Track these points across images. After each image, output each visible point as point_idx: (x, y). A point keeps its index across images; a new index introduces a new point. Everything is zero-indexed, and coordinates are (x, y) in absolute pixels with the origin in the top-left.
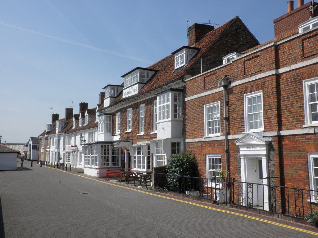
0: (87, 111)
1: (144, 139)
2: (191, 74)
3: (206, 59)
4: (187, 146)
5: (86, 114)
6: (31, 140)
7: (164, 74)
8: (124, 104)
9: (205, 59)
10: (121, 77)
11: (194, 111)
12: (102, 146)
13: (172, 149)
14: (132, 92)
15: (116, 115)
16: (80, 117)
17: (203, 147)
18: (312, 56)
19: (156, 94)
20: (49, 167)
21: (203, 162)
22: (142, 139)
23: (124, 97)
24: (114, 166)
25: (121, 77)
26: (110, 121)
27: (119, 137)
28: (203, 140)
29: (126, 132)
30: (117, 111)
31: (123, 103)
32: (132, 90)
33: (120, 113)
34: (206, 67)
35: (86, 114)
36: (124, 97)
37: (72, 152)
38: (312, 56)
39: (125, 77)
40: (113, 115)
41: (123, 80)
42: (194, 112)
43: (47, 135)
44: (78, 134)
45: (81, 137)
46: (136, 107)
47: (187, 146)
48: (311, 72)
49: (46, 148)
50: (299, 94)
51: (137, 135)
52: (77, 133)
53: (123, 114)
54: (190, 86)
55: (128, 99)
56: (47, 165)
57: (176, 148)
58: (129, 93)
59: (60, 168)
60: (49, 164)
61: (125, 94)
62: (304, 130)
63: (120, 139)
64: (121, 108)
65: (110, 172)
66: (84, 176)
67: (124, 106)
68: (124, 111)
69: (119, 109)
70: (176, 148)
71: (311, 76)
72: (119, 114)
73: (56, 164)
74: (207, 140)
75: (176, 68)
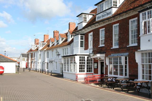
6: (21, 55)
8: (97, 25)
10: (95, 5)
12: (80, 57)
14: (106, 15)
18: (102, 8)
19: (139, 12)
24: (88, 73)
25: (95, 5)
26: (83, 39)
31: (97, 24)
32: (106, 13)
33: (92, 32)
37: (50, 62)
38: (102, 8)
44: (54, 50)
50: (111, 42)
51: (111, 48)
56: (36, 71)
57: (89, 70)
70: (89, 70)
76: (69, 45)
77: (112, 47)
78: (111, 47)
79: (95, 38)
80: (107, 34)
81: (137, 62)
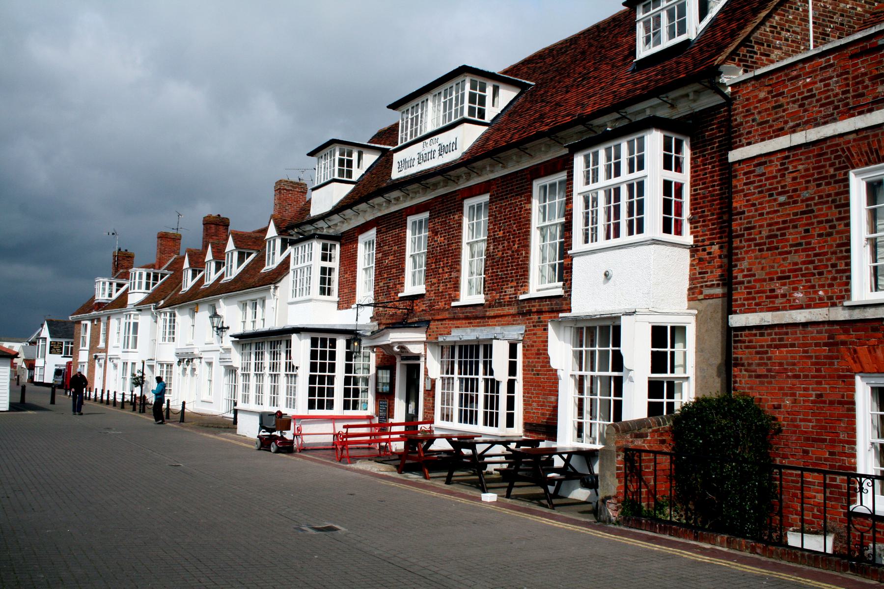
0: (212, 248)
1: (483, 317)
2: (740, 60)
3: (791, 11)
4: (736, 342)
5: (230, 245)
7: (585, 77)
8: (397, 199)
9: (787, 11)
11: (782, 199)
12: (314, 342)
13: (653, 354)
15: (356, 241)
16: (209, 256)
17: (836, 344)
20: (101, 406)
21: (842, 410)
22: (476, 318)
23: (395, 174)
27: (369, 312)
28: (839, 314)
29: (400, 295)
30: (364, 228)
31: (395, 194)
32: (436, 147)
34: (793, 41)
35: (230, 245)
36: (395, 174)
39: (404, 108)
40: (348, 240)
41: (395, 117)
42: (781, 205)
43: (97, 310)
45: (215, 315)
46: (444, 213)
47: (736, 342)
48: (873, 146)
49: (93, 348)
51: (454, 304)
52: (197, 304)
53: (388, 237)
54: (760, 101)
55: (421, 179)
58: (422, 158)
59: (144, 411)
60: (105, 398)
61: (405, 163)
62: (593, 310)
63: (372, 321)
64: (379, 214)
65: (351, 431)
66: (236, 440)
67: (394, 209)
68: (390, 228)
69: (370, 217)
71: (874, 157)
72: (372, 234)
73: (128, 398)
74: (857, 315)
75: (643, 51)
76: (272, 287)
77: (458, 300)
78: (454, 300)
79: (386, 255)
80: (439, 239)
81: (554, 364)
